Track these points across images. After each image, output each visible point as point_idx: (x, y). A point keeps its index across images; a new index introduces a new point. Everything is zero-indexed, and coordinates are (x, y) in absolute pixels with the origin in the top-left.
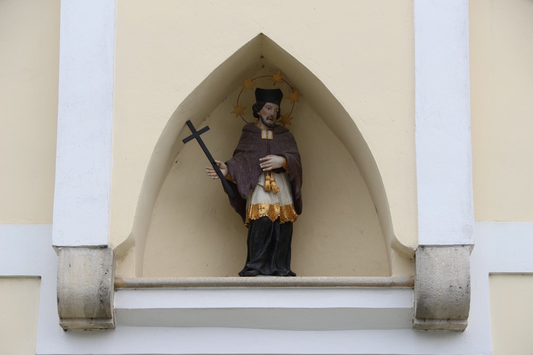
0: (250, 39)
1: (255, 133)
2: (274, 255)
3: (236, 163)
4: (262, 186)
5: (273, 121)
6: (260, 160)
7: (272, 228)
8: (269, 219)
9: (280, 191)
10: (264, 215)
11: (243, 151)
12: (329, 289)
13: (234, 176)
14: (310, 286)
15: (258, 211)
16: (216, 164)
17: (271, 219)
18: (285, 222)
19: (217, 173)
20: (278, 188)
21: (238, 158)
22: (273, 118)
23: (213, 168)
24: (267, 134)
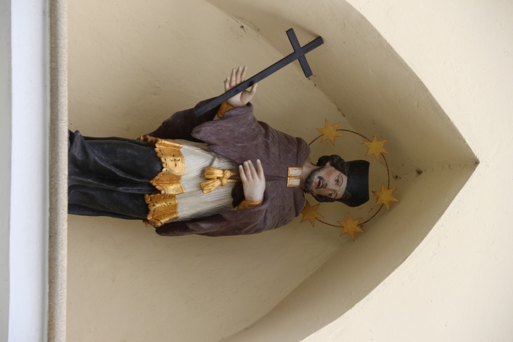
0: (469, 142)
1: (297, 156)
2: (93, 182)
3: (248, 122)
4: (211, 164)
5: (316, 188)
6: (259, 161)
7: (141, 180)
8: (158, 173)
9: (204, 194)
10: (164, 165)
11: (266, 136)
12: (43, 270)
13: (230, 116)
14: (50, 236)
15: (170, 155)
16: (250, 86)
17: (157, 178)
18: (148, 204)
19: (234, 87)
20: (210, 191)
21: (256, 126)
22: (322, 187)
23: (243, 80)
24: (295, 177)
